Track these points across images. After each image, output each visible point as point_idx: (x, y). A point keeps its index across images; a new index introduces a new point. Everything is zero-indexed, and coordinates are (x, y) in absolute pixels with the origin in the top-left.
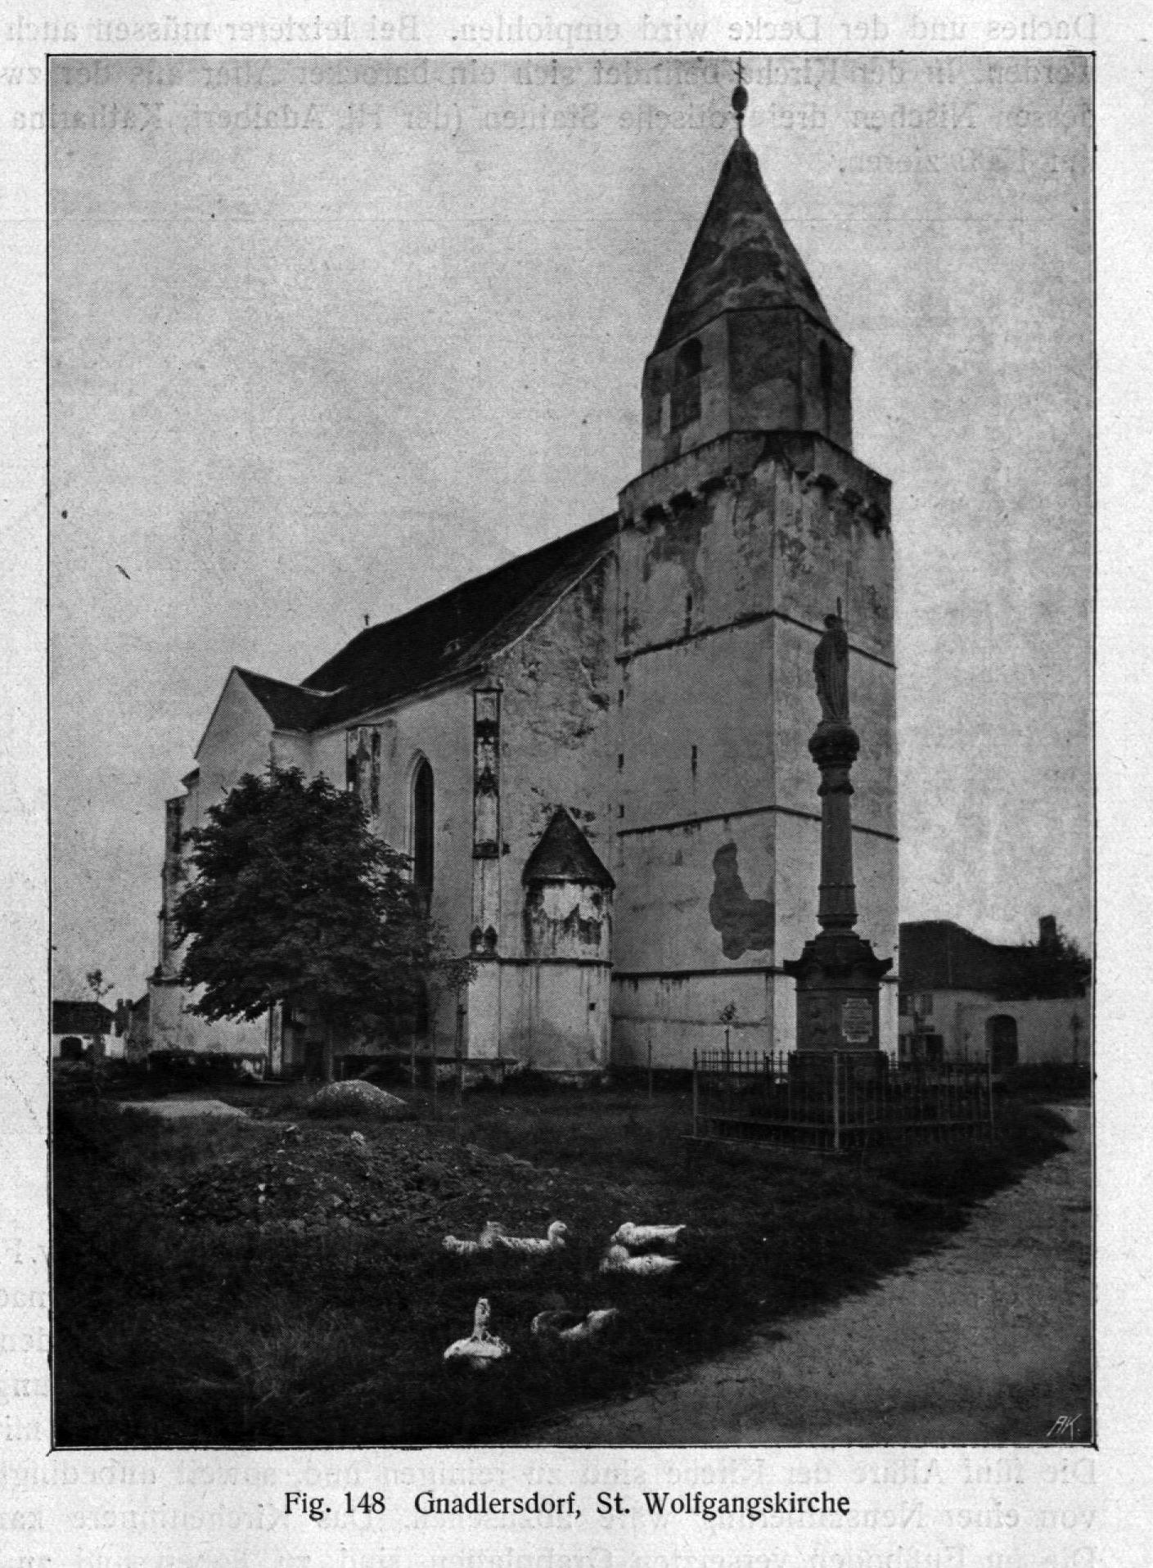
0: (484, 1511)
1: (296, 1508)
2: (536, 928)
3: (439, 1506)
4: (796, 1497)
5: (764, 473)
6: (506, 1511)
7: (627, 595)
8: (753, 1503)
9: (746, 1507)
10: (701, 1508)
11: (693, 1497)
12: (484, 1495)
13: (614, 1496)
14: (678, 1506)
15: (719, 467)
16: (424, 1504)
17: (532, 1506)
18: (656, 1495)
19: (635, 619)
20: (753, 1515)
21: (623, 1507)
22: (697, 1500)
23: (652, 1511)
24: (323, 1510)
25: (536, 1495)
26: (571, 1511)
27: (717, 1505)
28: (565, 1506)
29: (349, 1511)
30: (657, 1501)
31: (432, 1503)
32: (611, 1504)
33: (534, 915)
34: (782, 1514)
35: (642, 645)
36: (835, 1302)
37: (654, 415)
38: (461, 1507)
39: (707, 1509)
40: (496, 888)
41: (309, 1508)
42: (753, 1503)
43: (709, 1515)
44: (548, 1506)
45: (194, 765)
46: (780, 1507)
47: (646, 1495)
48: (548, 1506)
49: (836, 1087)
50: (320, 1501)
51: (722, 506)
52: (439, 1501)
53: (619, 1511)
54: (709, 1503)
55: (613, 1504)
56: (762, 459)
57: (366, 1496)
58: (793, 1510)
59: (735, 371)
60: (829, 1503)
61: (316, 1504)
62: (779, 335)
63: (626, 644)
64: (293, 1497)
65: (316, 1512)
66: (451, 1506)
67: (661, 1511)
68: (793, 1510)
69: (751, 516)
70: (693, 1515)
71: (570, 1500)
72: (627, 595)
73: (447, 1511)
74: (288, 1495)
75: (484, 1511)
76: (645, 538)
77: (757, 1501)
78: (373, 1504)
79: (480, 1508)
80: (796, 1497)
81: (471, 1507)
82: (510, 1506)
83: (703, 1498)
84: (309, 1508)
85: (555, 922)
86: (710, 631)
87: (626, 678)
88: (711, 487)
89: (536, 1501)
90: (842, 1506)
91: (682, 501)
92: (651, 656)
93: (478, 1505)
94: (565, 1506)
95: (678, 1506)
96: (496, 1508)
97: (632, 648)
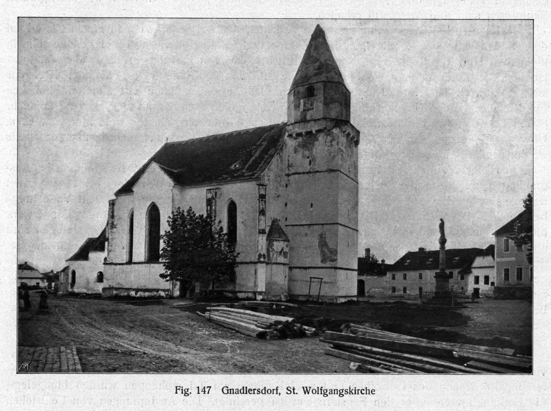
1: (179, 392)
2: (271, 254)
3: (230, 391)
4: (357, 389)
5: (336, 131)
6: (254, 393)
7: (289, 156)
8: (341, 391)
9: (339, 393)
10: (323, 392)
11: (320, 388)
12: (246, 387)
13: (292, 388)
14: (314, 392)
15: (321, 127)
16: (225, 391)
17: (264, 391)
18: (306, 387)
19: (292, 164)
20: (341, 395)
21: (295, 392)
22: (321, 390)
23: (305, 393)
26: (277, 393)
27: (328, 392)
28: (275, 391)
29: (199, 393)
30: (307, 390)
31: (228, 390)
32: (291, 391)
33: (271, 250)
34: (351, 395)
35: (294, 172)
36: (171, 178)
38: (238, 392)
39: (324, 393)
41: (184, 392)
42: (341, 391)
43: (325, 395)
44: (269, 392)
45: (114, 197)
46: (351, 392)
47: (303, 388)
48: (269, 392)
50: (188, 389)
51: (321, 138)
52: (230, 390)
53: (294, 393)
54: (325, 391)
55: (292, 391)
56: (335, 126)
57: (204, 388)
58: (355, 393)
59: (325, 98)
60: (368, 391)
61: (186, 390)
63: (289, 170)
64: (178, 388)
65: (186, 393)
66: (235, 391)
67: (308, 393)
68: (355, 393)
69: (331, 141)
70: (320, 395)
71: (277, 389)
72: (289, 156)
73: (233, 393)
74: (176, 387)
76: (295, 141)
77: (343, 390)
78: (206, 390)
80: (357, 389)
81: (242, 392)
82: (256, 391)
83: (323, 389)
84: (184, 392)
85: (277, 252)
86: (317, 172)
87: (289, 181)
88: (318, 131)
89: (265, 390)
90: (372, 392)
91: (309, 133)
92: (297, 176)
93: (246, 391)
94: (275, 391)
95: (314, 392)
97: (291, 173)
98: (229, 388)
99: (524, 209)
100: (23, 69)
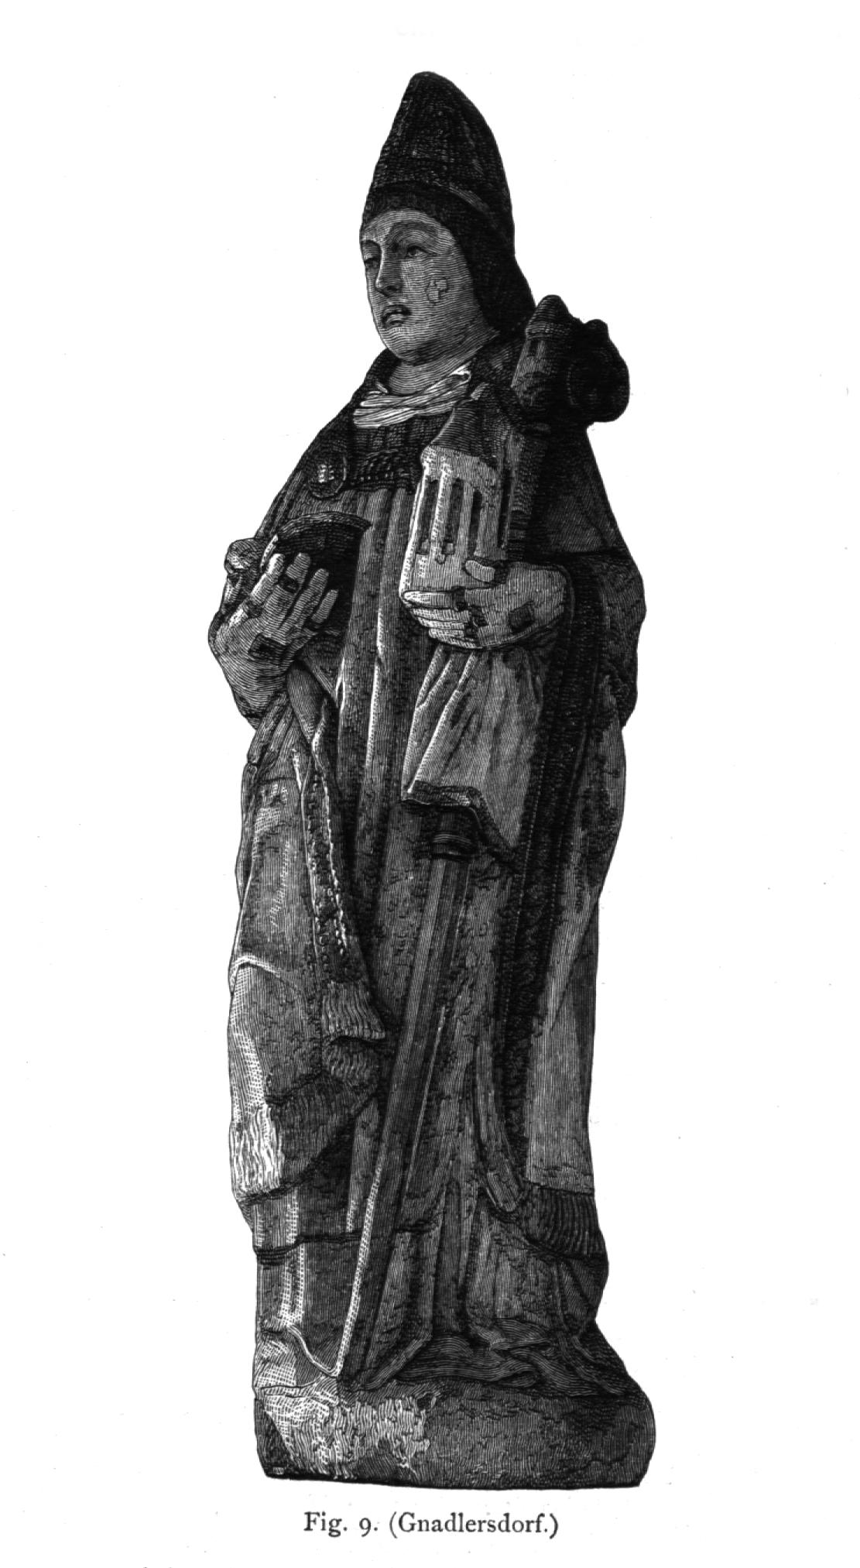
0: (507, 1530)
1: (316, 1527)
12: (461, 1515)
16: (547, 1523)
24: (340, 1528)
25: (507, 1515)
26: (538, 1531)
28: (533, 1527)
37: (471, 750)
40: (421, 1047)
44: (518, 1526)
48: (518, 1526)
49: (427, 1084)
50: (338, 1521)
62: (422, 561)
64: (313, 1517)
66: (431, 1526)
71: (538, 1522)
74: (309, 1514)
75: (507, 1530)
79: (458, 1527)
82: (485, 1526)
93: (507, 1524)
94: (533, 1527)
96: (471, 1527)
98: (417, 1517)
99: (538, 297)
100: (574, 1107)
